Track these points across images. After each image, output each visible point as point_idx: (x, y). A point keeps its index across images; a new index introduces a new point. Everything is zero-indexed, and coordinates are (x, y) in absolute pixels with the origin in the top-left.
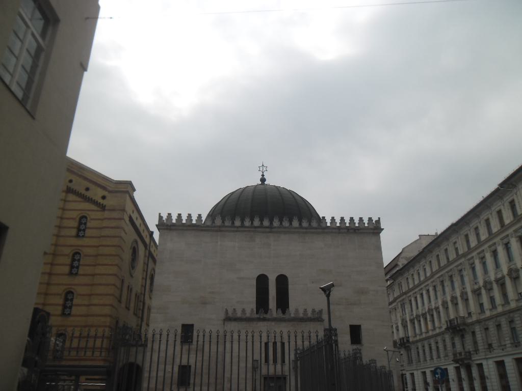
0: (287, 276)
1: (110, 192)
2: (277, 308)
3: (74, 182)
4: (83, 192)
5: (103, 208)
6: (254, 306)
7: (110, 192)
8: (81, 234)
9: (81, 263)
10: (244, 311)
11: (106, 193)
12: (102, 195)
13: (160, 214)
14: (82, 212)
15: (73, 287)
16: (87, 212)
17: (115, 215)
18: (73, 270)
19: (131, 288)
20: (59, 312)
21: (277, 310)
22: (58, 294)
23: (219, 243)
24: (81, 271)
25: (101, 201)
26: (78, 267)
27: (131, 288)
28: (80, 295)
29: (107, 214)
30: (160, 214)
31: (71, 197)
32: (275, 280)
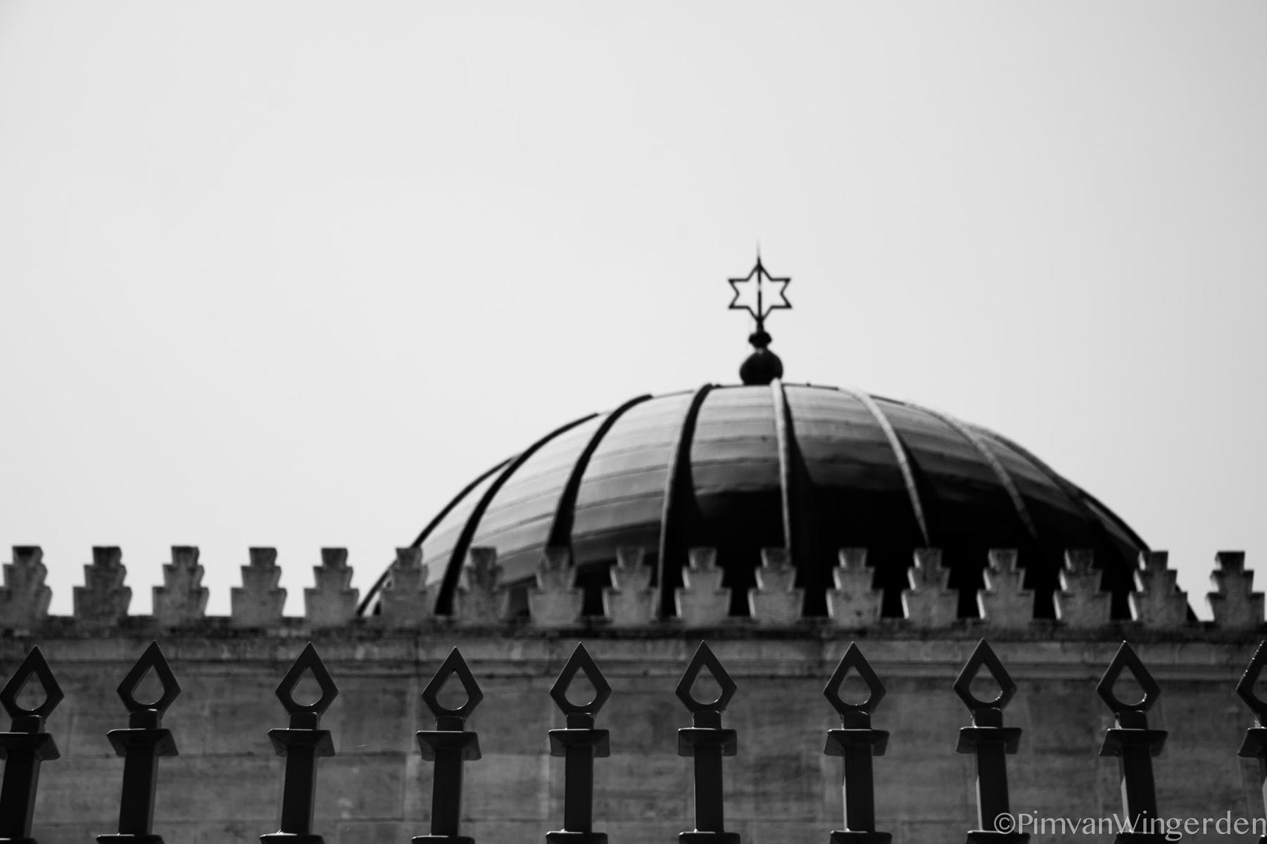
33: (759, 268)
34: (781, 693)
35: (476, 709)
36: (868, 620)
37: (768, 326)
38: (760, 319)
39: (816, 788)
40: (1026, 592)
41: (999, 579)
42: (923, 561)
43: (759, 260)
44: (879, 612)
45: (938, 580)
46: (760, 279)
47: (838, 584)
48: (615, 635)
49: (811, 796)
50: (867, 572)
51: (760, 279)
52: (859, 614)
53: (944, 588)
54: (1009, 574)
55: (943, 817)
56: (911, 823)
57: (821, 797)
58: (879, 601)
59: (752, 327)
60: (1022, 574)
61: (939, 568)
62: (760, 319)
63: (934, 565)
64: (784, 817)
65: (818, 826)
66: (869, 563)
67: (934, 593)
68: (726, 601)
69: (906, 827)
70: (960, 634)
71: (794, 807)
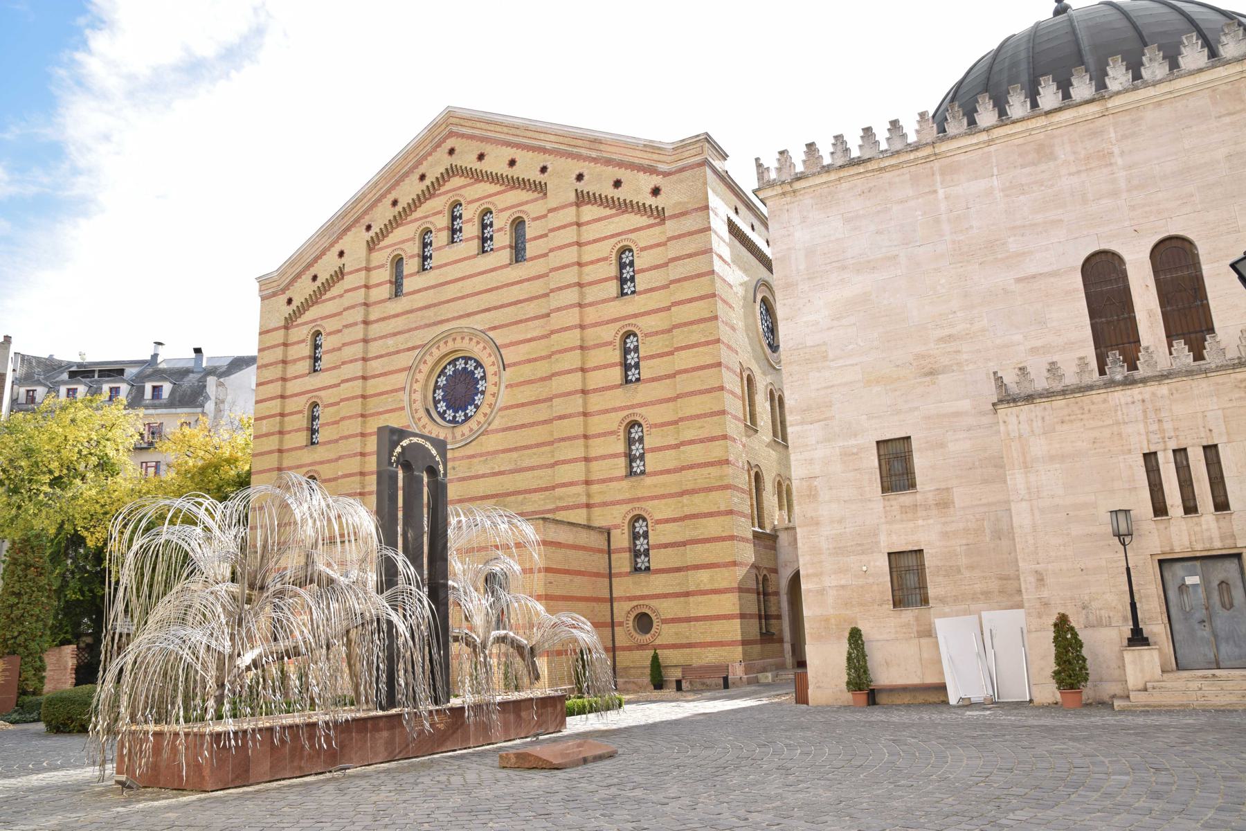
0: (1191, 236)
1: (666, 174)
2: (1170, 337)
3: (586, 178)
4: (610, 191)
5: (660, 215)
6: (1089, 351)
7: (666, 174)
8: (628, 288)
9: (642, 353)
10: (1053, 368)
11: (656, 180)
12: (652, 186)
13: (757, 160)
14: (619, 238)
15: (637, 410)
16: (630, 236)
17: (689, 224)
18: (628, 369)
19: (780, 396)
20: (622, 471)
21: (1170, 345)
22: (612, 433)
23: (941, 193)
24: (645, 373)
25: (651, 201)
26: (637, 366)
27: (780, 396)
28: (656, 426)
29: (671, 227)
30: (757, 160)
31: (589, 212)
32: (1148, 258)
34: (1091, 126)
36: (1126, 85)
39: (1113, 161)
41: (1187, 49)
57: (1116, 163)
67: (1156, 64)
69: (1157, 166)
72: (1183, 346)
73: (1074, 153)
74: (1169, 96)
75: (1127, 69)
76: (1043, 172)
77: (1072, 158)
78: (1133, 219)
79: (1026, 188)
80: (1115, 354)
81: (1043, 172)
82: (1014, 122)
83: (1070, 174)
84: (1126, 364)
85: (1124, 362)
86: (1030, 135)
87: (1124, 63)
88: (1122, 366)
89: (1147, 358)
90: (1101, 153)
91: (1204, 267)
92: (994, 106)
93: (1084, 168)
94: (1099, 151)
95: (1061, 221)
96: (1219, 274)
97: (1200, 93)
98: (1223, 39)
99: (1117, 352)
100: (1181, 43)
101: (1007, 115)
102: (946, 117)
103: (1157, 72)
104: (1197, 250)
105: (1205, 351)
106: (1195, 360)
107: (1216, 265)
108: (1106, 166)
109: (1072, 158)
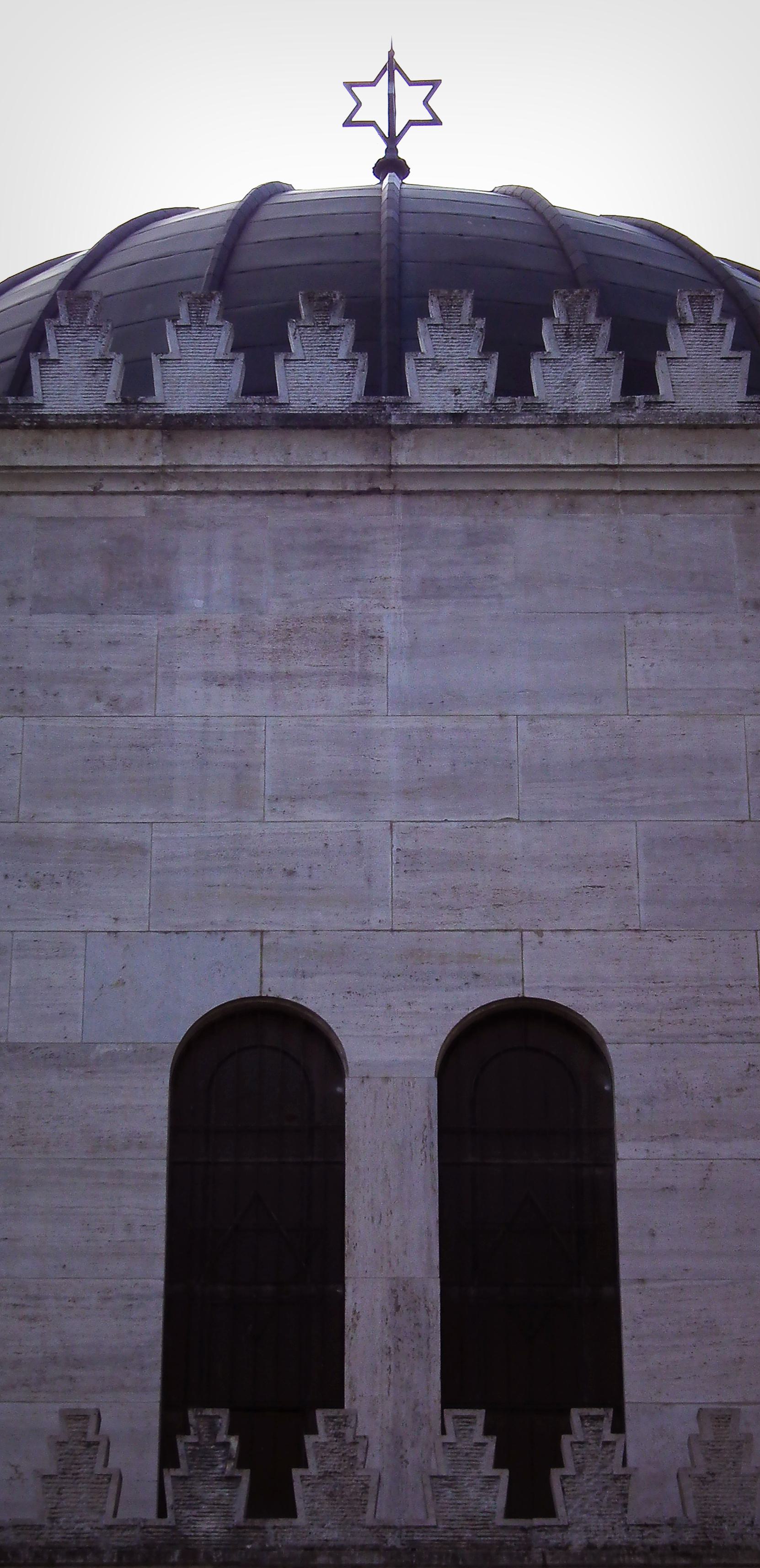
0: (596, 1020)
32: (432, 1073)
33: (391, 67)
34: (323, 516)
35: (522, 1520)
36: (470, 402)
37: (404, 150)
38: (392, 140)
39: (376, 666)
40: (735, 354)
41: (690, 335)
42: (568, 310)
43: (391, 54)
44: (491, 389)
45: (591, 338)
46: (391, 80)
47: (424, 343)
48: (43, 425)
49: (366, 678)
50: (472, 326)
51: (391, 80)
52: (457, 392)
53: (601, 348)
54: (710, 326)
55: (586, 709)
56: (532, 718)
57: (384, 679)
58: (491, 372)
59: (379, 150)
60: (731, 327)
61: (592, 319)
62: (392, 140)
63: (584, 315)
64: (321, 711)
65: (376, 723)
66: (476, 313)
67: (583, 358)
68: (236, 374)
69: (523, 725)
70: (623, 417)
71: (337, 694)
72: (478, 1436)
73: (243, 602)
74: (605, 484)
75: (488, 348)
76: (112, 643)
77: (228, 619)
78: (406, 905)
79: (33, 690)
80: (212, 1422)
81: (112, 643)
82: (43, 425)
83: (211, 679)
84: (245, 1475)
85: (241, 1464)
86: (95, 492)
87: (481, 323)
88: (232, 1480)
89: (332, 1463)
90: (339, 629)
91: (623, 1149)
92: (357, 347)
93: (266, 667)
94: (332, 618)
95: (141, 849)
96: (671, 1189)
97: (709, 501)
98: (673, 334)
99: (223, 1417)
100: (670, 308)
101: (655, 390)
102: (57, 310)
103: (582, 387)
104: (611, 1082)
105: (555, 1475)
106: (510, 1513)
107: (665, 1149)
108: (348, 679)
109: (228, 619)
